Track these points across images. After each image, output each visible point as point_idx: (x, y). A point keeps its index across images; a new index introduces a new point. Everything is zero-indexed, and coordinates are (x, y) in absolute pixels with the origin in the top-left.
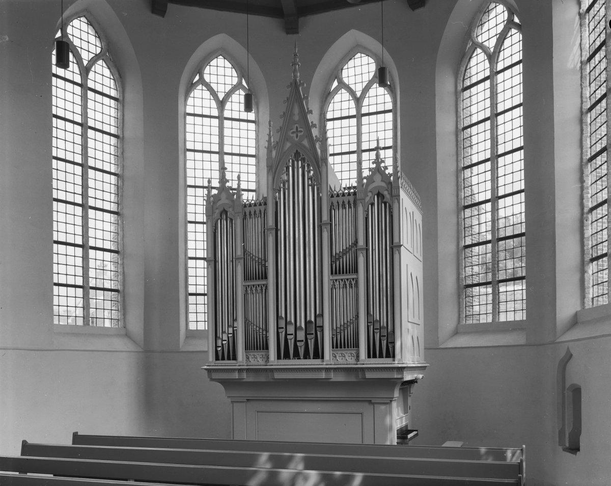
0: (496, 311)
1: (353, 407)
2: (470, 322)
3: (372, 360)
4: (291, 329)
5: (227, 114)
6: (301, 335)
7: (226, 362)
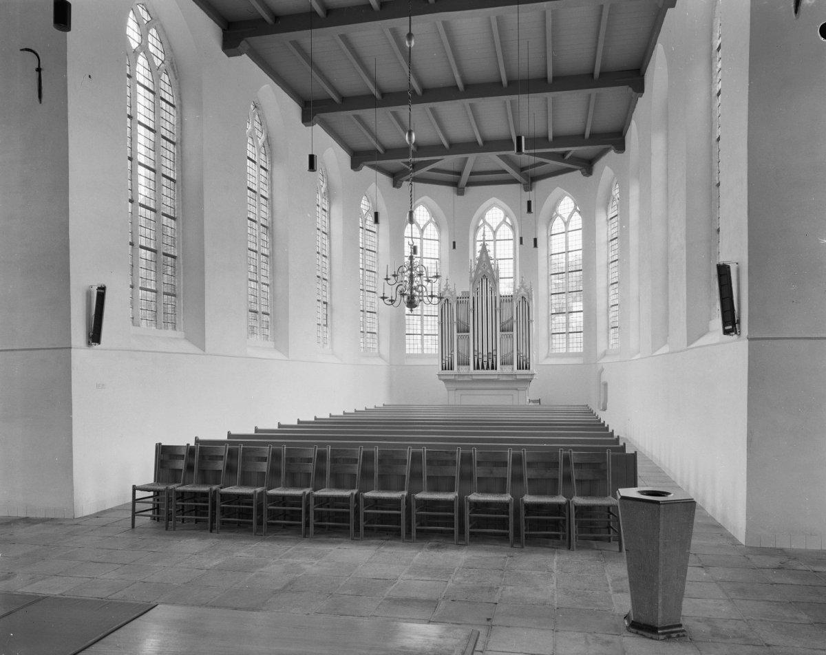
0: (568, 347)
1: (510, 392)
2: (554, 352)
3: (444, 371)
4: (480, 356)
5: (424, 237)
6: (485, 359)
7: (447, 371)
